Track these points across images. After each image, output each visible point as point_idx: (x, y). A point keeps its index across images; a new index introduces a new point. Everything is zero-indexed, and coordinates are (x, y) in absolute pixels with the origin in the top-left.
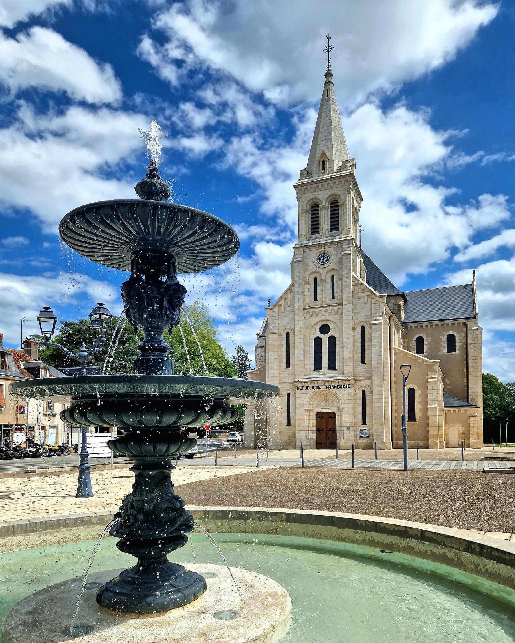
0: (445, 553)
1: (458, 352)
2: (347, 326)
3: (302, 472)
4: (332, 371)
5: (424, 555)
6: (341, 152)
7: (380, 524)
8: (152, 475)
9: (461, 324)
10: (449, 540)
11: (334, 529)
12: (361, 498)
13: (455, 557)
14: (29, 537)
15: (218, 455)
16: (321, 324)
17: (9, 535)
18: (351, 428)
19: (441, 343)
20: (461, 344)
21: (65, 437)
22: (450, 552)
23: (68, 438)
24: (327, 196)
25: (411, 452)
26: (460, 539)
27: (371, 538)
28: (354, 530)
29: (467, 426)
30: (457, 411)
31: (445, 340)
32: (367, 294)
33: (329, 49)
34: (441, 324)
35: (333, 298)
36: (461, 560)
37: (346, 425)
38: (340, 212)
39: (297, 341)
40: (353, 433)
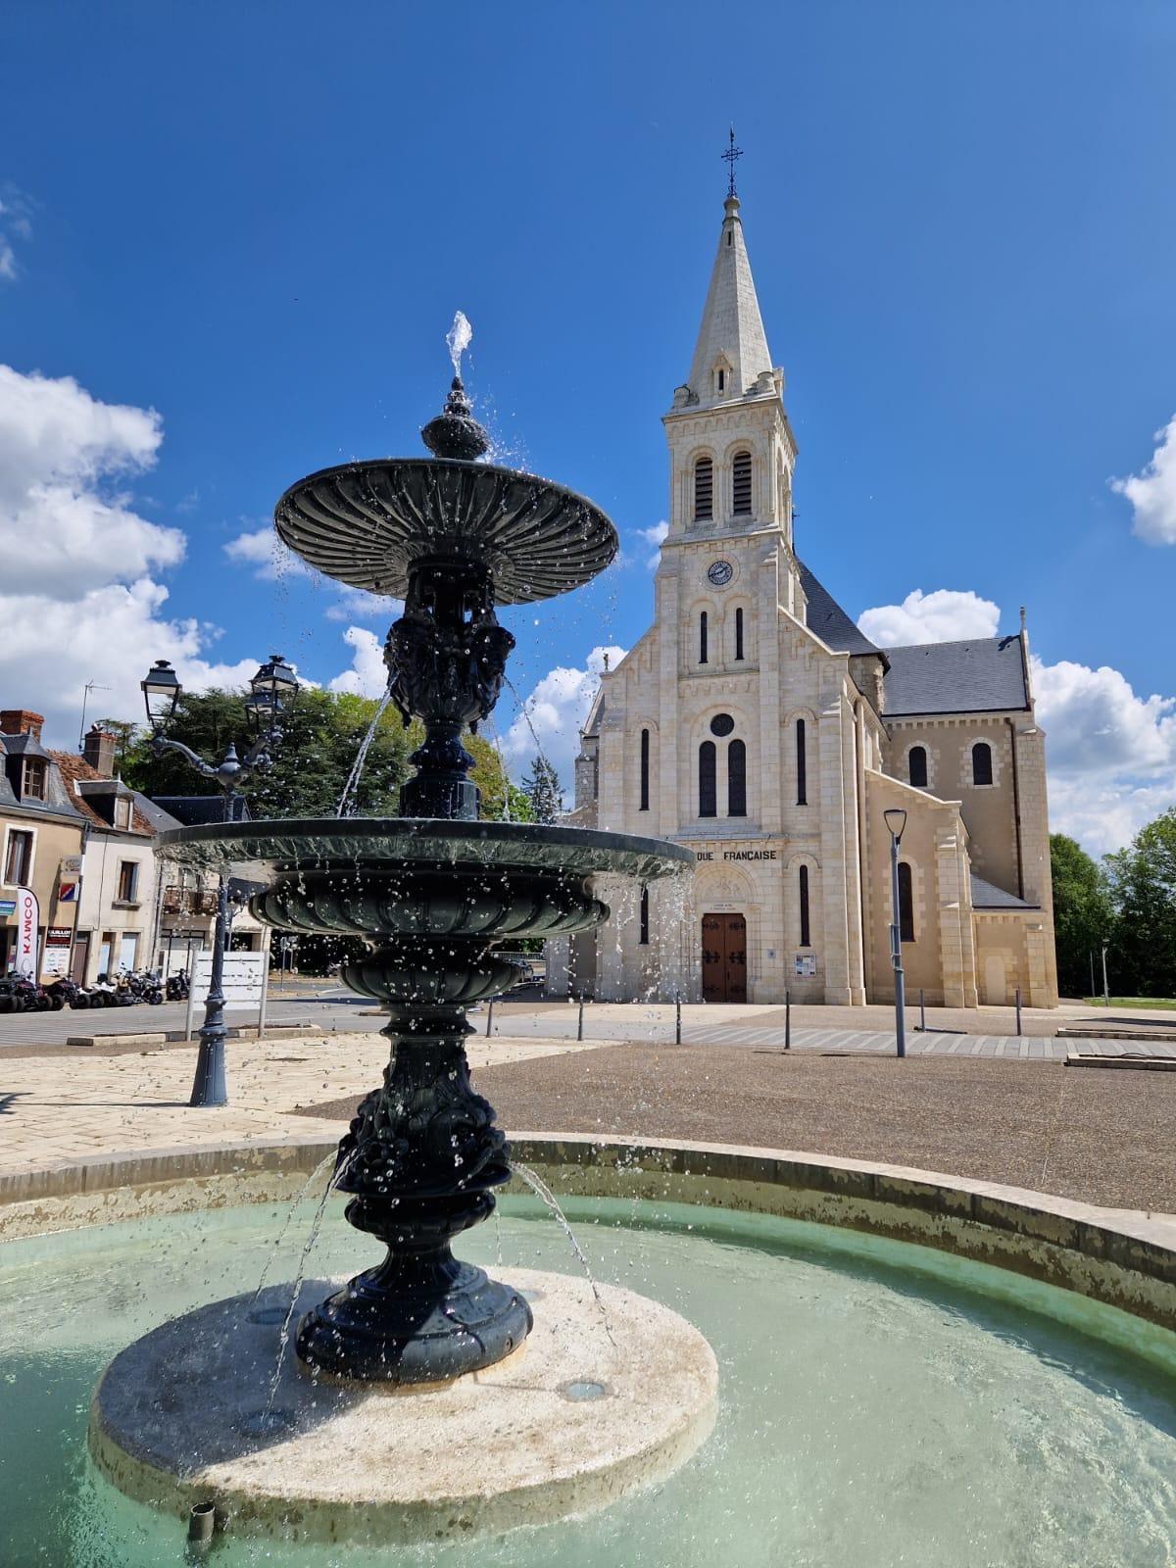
0: (1026, 1252)
1: (996, 783)
2: (769, 718)
3: (680, 1056)
4: (738, 820)
5: (979, 1254)
6: (755, 355)
7: (881, 1180)
8: (427, 1051)
9: (1002, 722)
10: (1034, 1220)
11: (780, 1192)
12: (815, 1120)
13: (1049, 1260)
14: (114, 1197)
15: (493, 1011)
16: (714, 713)
17: (75, 1191)
18: (778, 953)
19: (962, 762)
20: (1002, 765)
21: (156, 959)
22: (1036, 1248)
23: (161, 963)
24: (728, 441)
25: (911, 1014)
26: (1058, 1217)
27: (861, 1215)
28: (824, 1195)
29: (1022, 954)
30: (1000, 920)
31: (969, 756)
32: (809, 650)
33: (732, 155)
34: (961, 722)
35: (740, 656)
36: (1062, 1269)
37: (767, 946)
38: (753, 474)
39: (663, 750)
40: (781, 965)
